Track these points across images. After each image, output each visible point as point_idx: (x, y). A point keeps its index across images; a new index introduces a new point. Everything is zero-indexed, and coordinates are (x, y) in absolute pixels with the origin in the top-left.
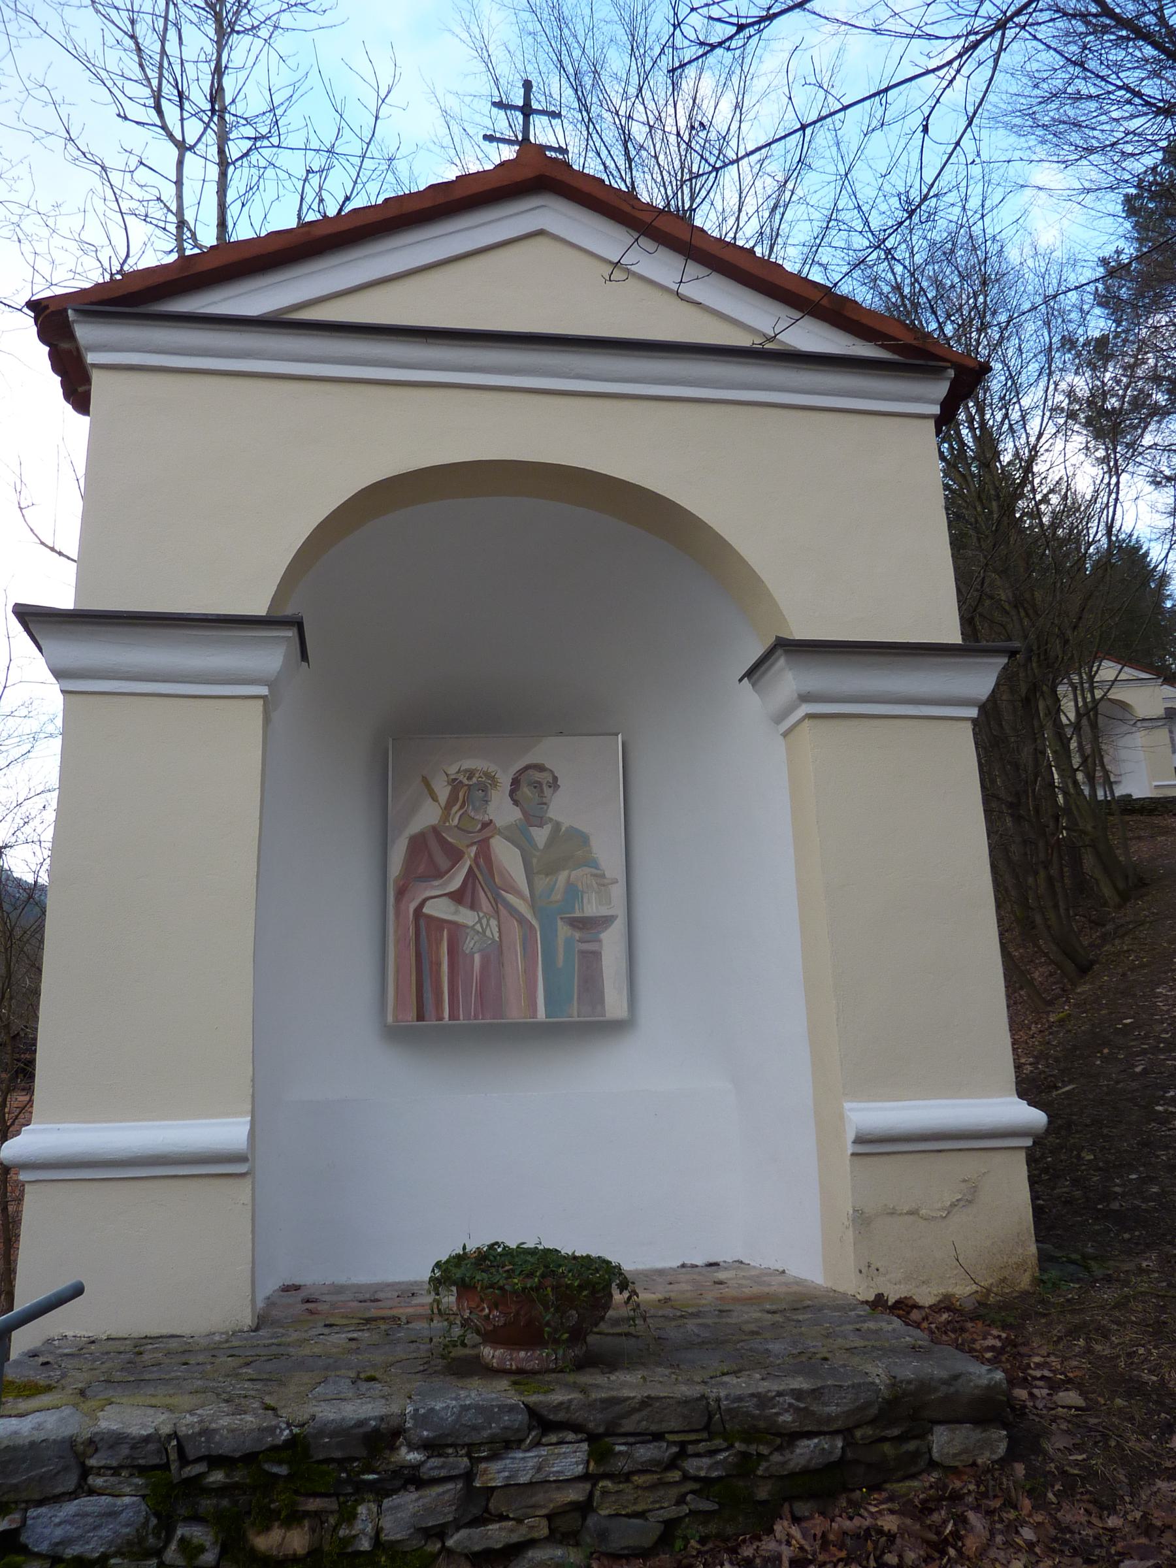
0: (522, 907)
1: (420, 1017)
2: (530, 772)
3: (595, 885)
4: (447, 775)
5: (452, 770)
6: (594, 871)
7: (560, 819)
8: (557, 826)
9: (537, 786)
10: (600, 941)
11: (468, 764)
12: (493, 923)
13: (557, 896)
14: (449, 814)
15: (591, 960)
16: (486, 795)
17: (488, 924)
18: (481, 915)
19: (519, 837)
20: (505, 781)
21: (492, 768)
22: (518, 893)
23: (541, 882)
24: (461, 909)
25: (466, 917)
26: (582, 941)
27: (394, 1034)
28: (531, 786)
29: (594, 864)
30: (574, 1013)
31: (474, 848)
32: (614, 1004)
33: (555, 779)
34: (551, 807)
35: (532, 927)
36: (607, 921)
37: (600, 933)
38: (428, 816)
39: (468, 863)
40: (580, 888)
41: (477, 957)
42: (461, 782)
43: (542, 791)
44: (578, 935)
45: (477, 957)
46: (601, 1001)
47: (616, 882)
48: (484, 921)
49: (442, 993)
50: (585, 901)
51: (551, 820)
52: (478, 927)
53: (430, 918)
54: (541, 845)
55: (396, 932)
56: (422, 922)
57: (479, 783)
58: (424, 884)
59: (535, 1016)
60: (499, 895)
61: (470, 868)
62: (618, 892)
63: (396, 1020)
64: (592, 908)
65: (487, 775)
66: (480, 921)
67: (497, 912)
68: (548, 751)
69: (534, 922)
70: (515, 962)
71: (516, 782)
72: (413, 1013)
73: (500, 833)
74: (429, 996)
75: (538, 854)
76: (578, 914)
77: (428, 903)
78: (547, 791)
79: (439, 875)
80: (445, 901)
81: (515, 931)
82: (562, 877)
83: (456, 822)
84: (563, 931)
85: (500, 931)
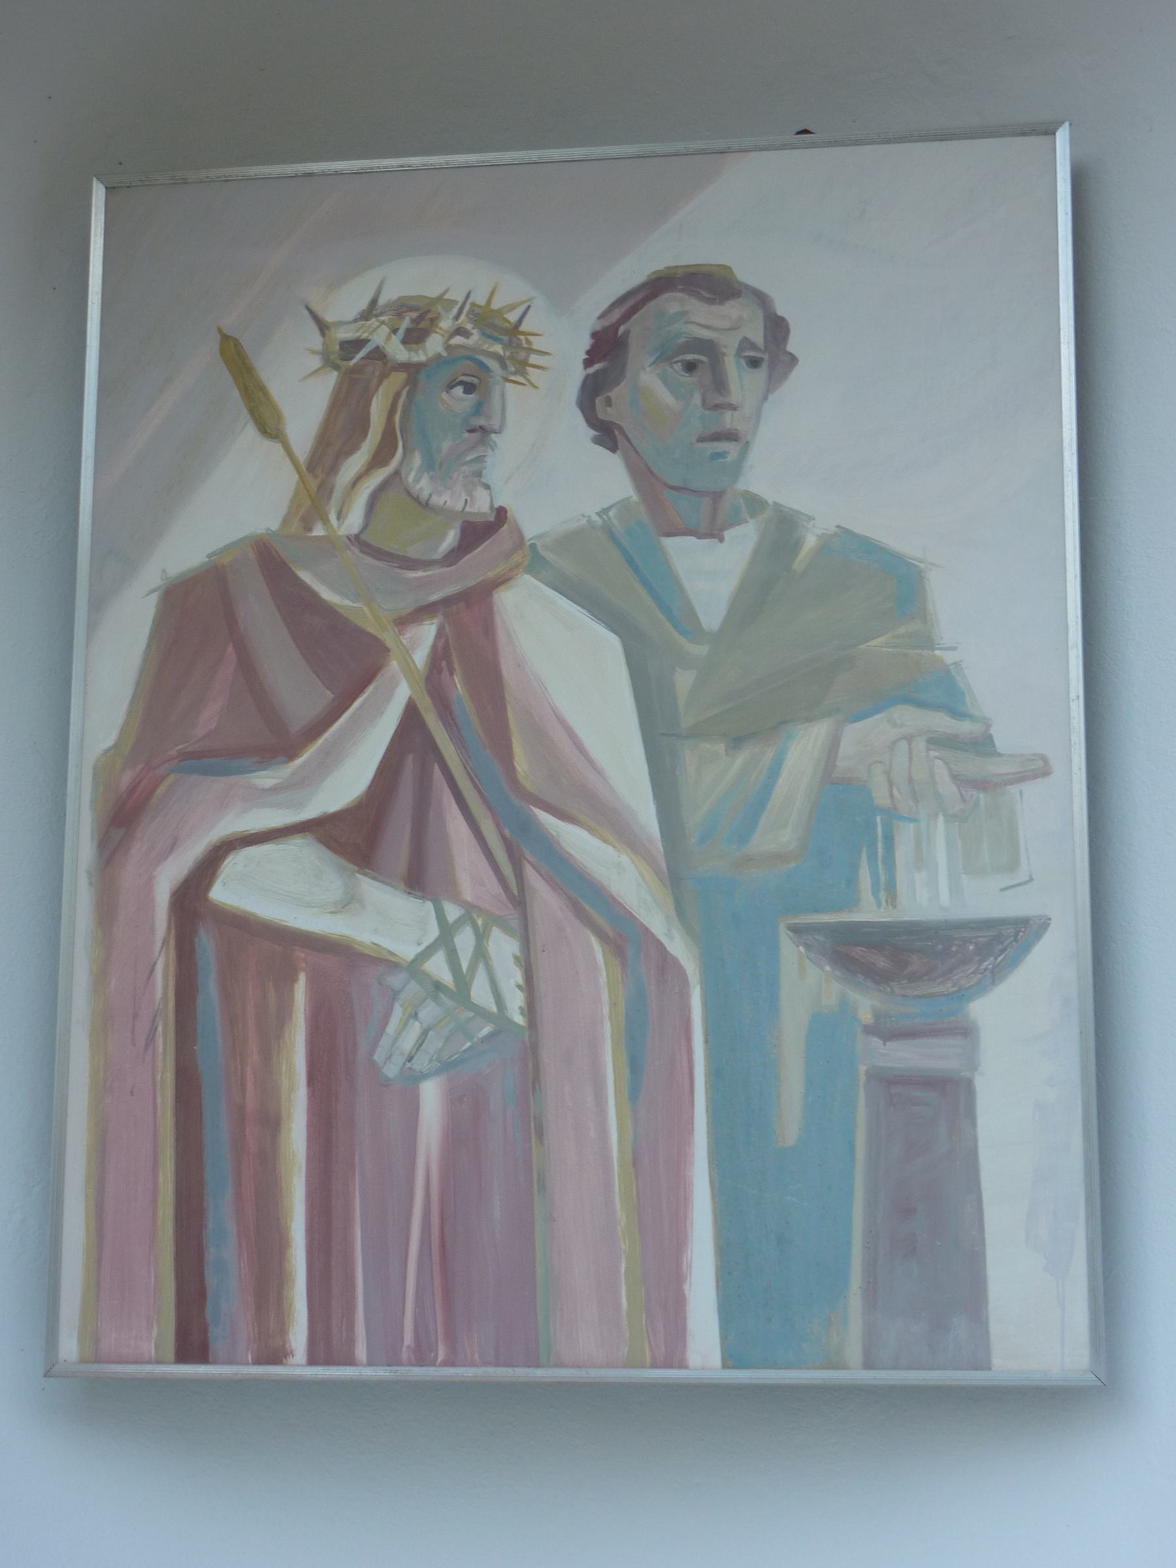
0: (627, 880)
1: (192, 1344)
2: (672, 303)
3: (948, 789)
4: (323, 327)
5: (344, 306)
6: (942, 723)
7: (794, 499)
8: (784, 528)
9: (699, 360)
10: (966, 1032)
11: (408, 278)
12: (504, 948)
13: (780, 832)
14: (325, 489)
15: (929, 1113)
16: (479, 409)
17: (480, 954)
18: (453, 912)
19: (617, 581)
20: (562, 344)
21: (504, 289)
22: (609, 820)
23: (711, 773)
24: (371, 889)
25: (387, 920)
26: (886, 1030)
27: (95, 1397)
28: (677, 360)
29: (940, 690)
30: (848, 1344)
31: (426, 634)
32: (1032, 1313)
33: (777, 328)
34: (755, 455)
35: (665, 963)
36: (999, 943)
37: (964, 995)
38: (241, 498)
39: (402, 693)
40: (881, 797)
41: (431, 1095)
42: (378, 354)
43: (720, 384)
44: (865, 1004)
45: (431, 1095)
46: (971, 1294)
47: (1037, 769)
48: (465, 941)
49: (282, 1245)
50: (903, 854)
51: (755, 504)
52: (437, 966)
53: (241, 926)
54: (712, 616)
55: (100, 978)
56: (207, 943)
57: (452, 355)
58: (215, 785)
59: (674, 1356)
60: (528, 827)
61: (411, 714)
62: (1051, 814)
63: (94, 1353)
64: (932, 886)
65: (486, 319)
66: (446, 940)
67: (520, 900)
68: (749, 216)
69: (678, 947)
70: (593, 1119)
71: (607, 347)
72: (162, 1329)
73: (536, 564)
74: (226, 1257)
75: (700, 650)
76: (869, 911)
77: (233, 864)
78: (742, 383)
79: (278, 742)
80: (303, 853)
81: (594, 982)
82: (803, 749)
83: (354, 520)
84: (805, 985)
85: (529, 985)
